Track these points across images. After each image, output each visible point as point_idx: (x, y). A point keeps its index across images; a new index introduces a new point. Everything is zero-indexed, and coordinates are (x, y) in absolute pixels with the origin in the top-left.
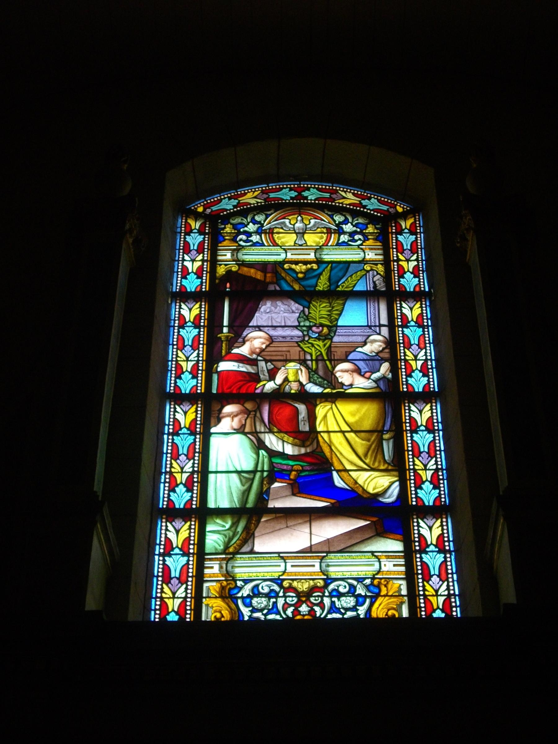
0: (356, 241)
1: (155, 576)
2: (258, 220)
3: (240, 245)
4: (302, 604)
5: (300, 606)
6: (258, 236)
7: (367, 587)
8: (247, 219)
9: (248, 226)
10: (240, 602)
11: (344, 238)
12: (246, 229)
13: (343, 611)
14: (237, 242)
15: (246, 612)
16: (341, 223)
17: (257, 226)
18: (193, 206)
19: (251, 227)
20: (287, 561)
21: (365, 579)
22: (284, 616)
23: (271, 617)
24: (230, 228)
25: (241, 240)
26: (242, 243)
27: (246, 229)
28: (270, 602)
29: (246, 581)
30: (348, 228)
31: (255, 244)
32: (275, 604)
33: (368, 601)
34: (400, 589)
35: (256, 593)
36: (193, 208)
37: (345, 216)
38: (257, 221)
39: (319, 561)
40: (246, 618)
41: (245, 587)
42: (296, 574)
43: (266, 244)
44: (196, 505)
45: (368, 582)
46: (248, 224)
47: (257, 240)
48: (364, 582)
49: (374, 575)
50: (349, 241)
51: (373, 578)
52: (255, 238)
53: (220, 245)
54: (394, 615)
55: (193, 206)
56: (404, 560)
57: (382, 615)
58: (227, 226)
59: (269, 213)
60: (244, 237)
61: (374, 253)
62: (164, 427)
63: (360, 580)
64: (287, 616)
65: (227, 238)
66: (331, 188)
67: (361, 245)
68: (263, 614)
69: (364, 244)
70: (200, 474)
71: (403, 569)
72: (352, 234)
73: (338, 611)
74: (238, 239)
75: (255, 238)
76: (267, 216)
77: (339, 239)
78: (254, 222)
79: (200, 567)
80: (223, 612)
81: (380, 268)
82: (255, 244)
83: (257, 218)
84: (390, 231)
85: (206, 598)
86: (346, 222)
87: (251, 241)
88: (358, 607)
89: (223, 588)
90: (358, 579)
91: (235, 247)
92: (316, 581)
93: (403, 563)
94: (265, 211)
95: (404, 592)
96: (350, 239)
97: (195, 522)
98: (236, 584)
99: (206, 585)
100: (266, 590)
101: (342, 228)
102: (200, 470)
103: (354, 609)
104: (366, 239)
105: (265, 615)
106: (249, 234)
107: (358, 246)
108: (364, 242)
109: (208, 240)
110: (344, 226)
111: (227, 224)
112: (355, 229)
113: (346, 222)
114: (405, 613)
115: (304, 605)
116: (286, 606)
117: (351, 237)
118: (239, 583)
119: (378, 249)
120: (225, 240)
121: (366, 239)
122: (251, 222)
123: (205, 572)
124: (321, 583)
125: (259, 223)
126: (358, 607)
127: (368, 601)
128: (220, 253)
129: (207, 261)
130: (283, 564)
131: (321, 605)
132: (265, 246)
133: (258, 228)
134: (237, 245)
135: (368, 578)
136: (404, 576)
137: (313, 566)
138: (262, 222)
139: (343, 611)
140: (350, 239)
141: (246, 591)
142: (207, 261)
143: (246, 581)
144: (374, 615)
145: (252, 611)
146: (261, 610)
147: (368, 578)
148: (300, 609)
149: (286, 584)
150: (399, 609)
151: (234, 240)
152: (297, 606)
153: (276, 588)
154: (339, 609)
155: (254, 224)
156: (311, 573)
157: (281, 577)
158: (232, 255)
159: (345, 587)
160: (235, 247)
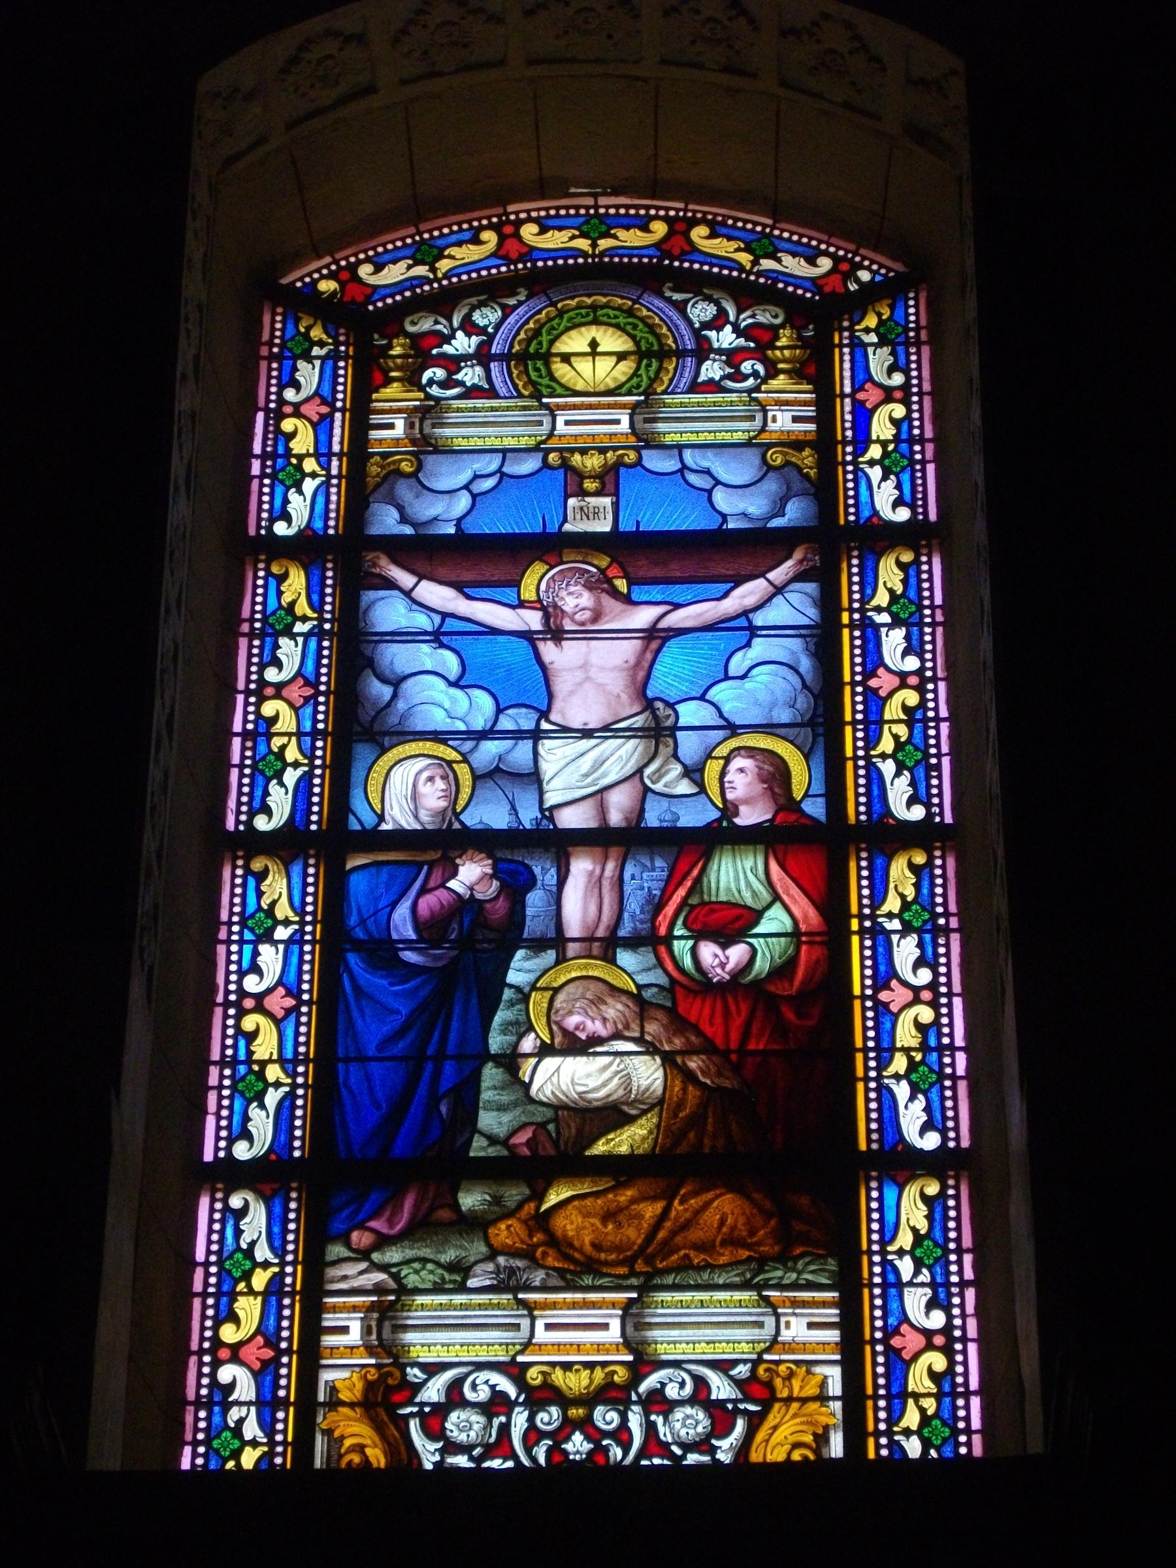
0: (745, 378)
1: (194, 1353)
2: (481, 324)
3: (428, 397)
4: (573, 1433)
5: (568, 1439)
6: (479, 370)
7: (738, 1383)
8: (450, 321)
9: (453, 342)
10: (414, 1426)
11: (712, 370)
12: (447, 348)
13: (677, 1450)
14: (422, 388)
15: (428, 1453)
16: (706, 325)
17: (475, 340)
18: (299, 280)
19: (463, 344)
20: (536, 1313)
21: (735, 1363)
22: (526, 1462)
23: (496, 1464)
24: (402, 346)
25: (431, 382)
26: (435, 391)
27: (447, 348)
28: (492, 1427)
29: (432, 1369)
30: (726, 338)
31: (472, 392)
32: (505, 1429)
33: (740, 1425)
34: (823, 1384)
35: (455, 1397)
36: (299, 284)
37: (717, 303)
38: (477, 326)
39: (620, 1312)
40: (429, 1466)
41: (430, 1384)
42: (559, 1347)
43: (502, 391)
44: (319, 823)
45: (742, 1371)
46: (452, 336)
47: (476, 381)
48: (733, 1373)
49: (760, 1354)
50: (723, 378)
51: (756, 1363)
52: (471, 375)
53: (374, 396)
54: (806, 1458)
55: (299, 280)
56: (837, 1311)
57: (778, 1455)
58: (395, 341)
59: (512, 302)
60: (440, 373)
61: (788, 415)
62: (228, 774)
63: (723, 1366)
64: (534, 1459)
65: (393, 374)
66: (681, 214)
67: (757, 389)
68: (471, 1458)
69: (763, 387)
70: (329, 739)
71: (833, 1335)
72: (732, 357)
73: (664, 1449)
74: (424, 381)
75: (471, 375)
76: (507, 311)
77: (697, 373)
78: (469, 327)
79: (312, 1330)
80: (368, 1451)
81: (807, 458)
82: (472, 392)
83: (478, 318)
84: (837, 341)
85: (347, 1060)
86: (720, 322)
87: (461, 383)
88: (714, 1442)
89: (369, 1386)
90: (714, 1365)
91: (418, 403)
92: (612, 1368)
93: (837, 1320)
94: (502, 297)
95: (835, 1387)
96: (729, 370)
97: (316, 866)
98: (404, 1374)
99: (326, 1376)
100: (483, 1394)
101: (707, 340)
102: (330, 729)
103: (703, 1445)
104: (772, 371)
105: (479, 1460)
106: (453, 363)
107: (750, 391)
108: (765, 381)
109: (333, 595)
110: (712, 334)
111: (397, 337)
112: (741, 342)
113: (717, 323)
114: (836, 1447)
115: (578, 1437)
116: (533, 1435)
117: (730, 366)
118: (415, 1374)
119: (805, 403)
120: (388, 381)
121: (772, 372)
122: (462, 327)
123: (324, 1344)
124: (621, 1375)
125: (482, 331)
126: (714, 1442)
127: (740, 1425)
128: (329, 1320)
129: (324, 734)
130: (525, 1323)
131: (622, 1435)
132: (496, 396)
133: (480, 346)
134: (421, 395)
135: (745, 1361)
136: (837, 1357)
137: (605, 1326)
138: (490, 330)
139: (677, 1450)
140: (729, 370)
141: (433, 1392)
142: (324, 734)
143: (432, 1369)
144: (755, 1457)
145: (443, 1451)
146: (466, 1449)
147: (745, 1361)
148: (569, 1447)
149: (533, 1376)
150: (822, 1439)
151: (412, 380)
152: (560, 1435)
153: (507, 1386)
154: (668, 1445)
155: (469, 335)
156: (599, 1347)
157: (520, 1359)
158: (410, 425)
159: (682, 1384)
160: (418, 403)
